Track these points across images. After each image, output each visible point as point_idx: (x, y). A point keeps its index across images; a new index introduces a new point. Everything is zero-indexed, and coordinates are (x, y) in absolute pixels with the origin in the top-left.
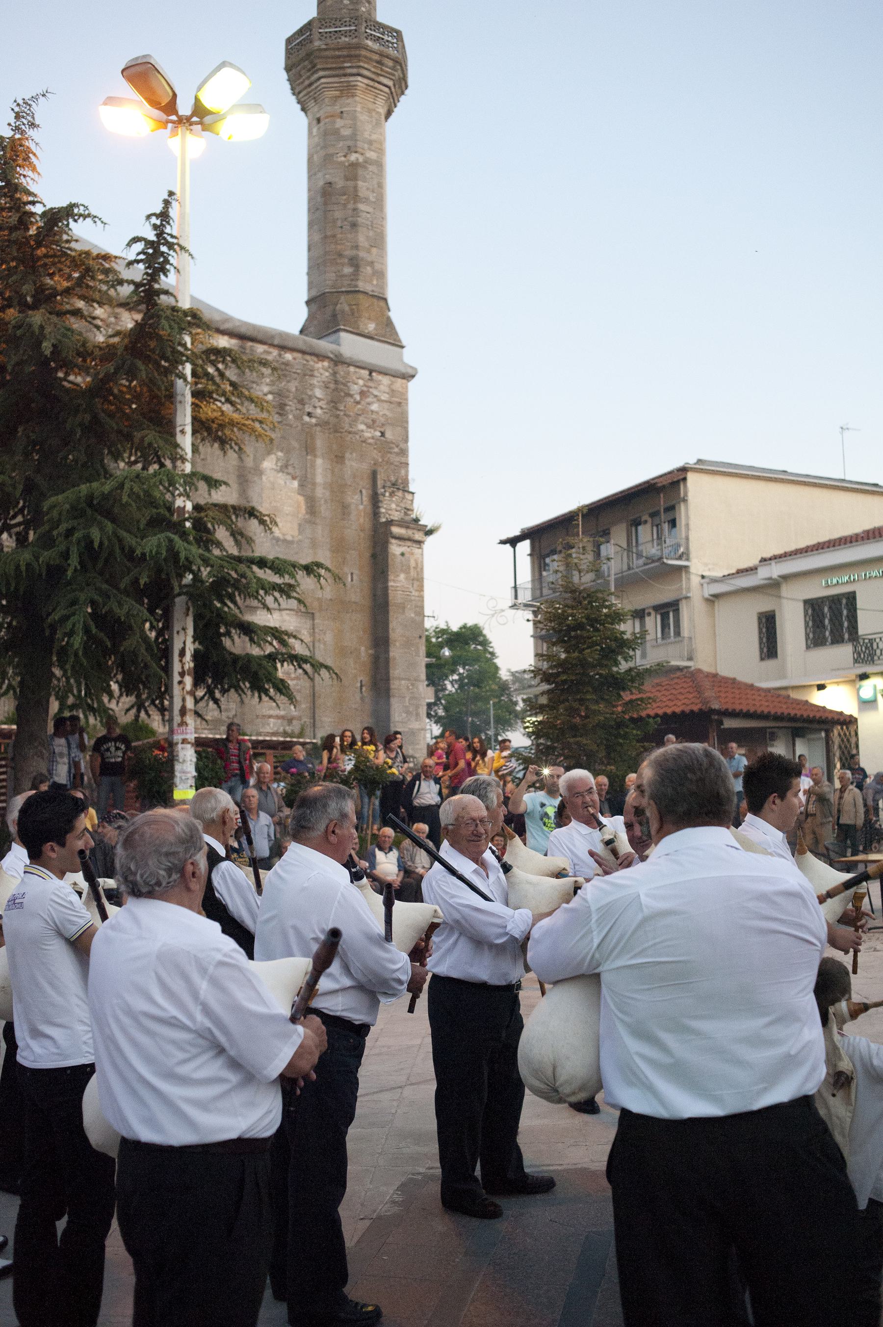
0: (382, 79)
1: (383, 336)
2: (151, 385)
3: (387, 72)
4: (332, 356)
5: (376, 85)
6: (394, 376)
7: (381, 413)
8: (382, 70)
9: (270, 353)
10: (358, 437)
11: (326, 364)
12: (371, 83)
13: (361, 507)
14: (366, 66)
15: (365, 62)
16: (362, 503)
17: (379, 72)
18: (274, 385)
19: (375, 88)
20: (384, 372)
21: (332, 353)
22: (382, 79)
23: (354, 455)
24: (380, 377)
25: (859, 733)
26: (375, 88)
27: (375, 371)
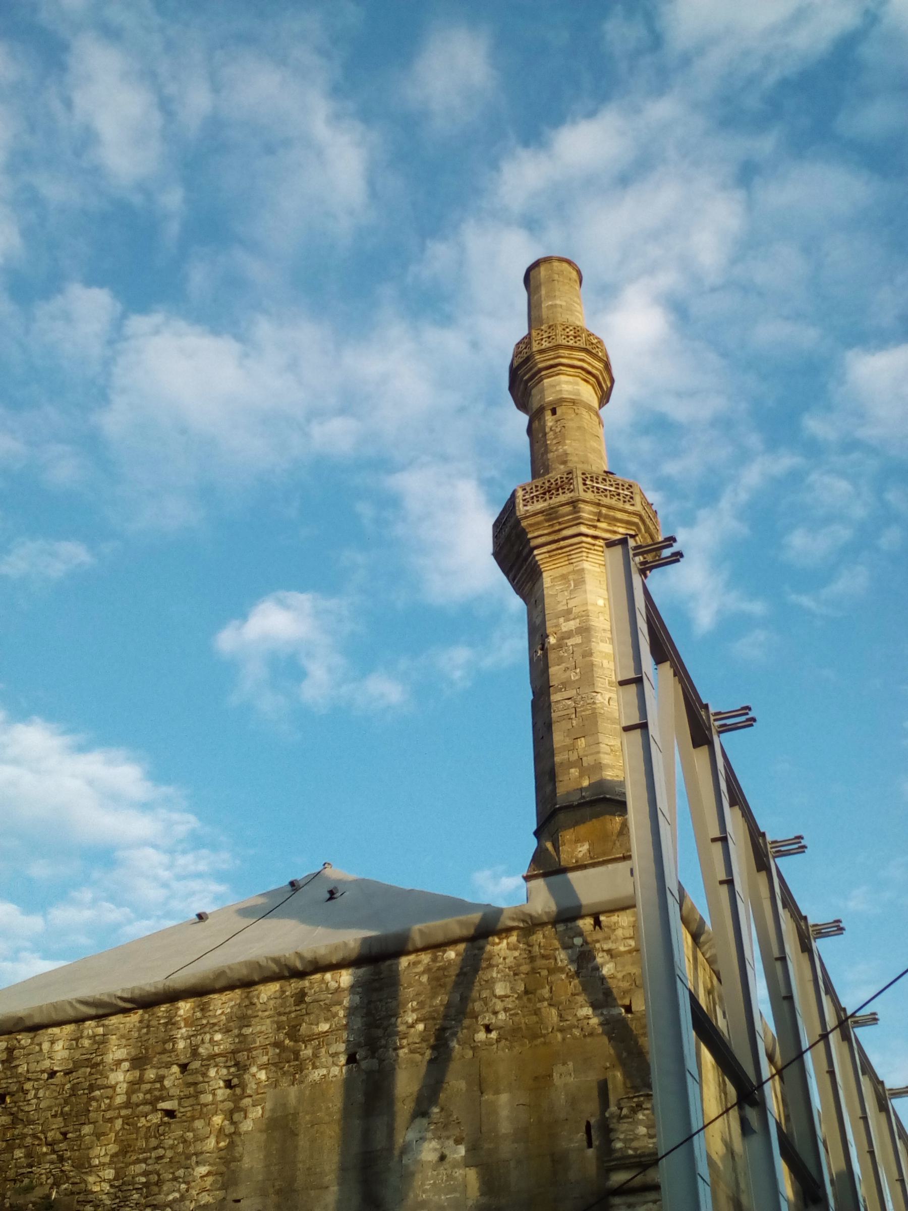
0: (566, 533)
1: (604, 854)
2: (512, 1012)
3: (569, 521)
4: (515, 924)
5: (562, 543)
6: (10, 1033)
7: (620, 975)
8: (560, 523)
9: (419, 962)
10: (577, 1032)
11: (513, 938)
12: (554, 546)
13: (590, 1152)
14: (536, 534)
15: (533, 531)
16: (590, 1145)
17: (557, 528)
18: (423, 1008)
19: (561, 548)
20: (172, 996)
21: (513, 919)
22: (566, 533)
23: (571, 1064)
24: (615, 918)
25: (585, 383)
26: (561, 548)
27: (603, 912)
